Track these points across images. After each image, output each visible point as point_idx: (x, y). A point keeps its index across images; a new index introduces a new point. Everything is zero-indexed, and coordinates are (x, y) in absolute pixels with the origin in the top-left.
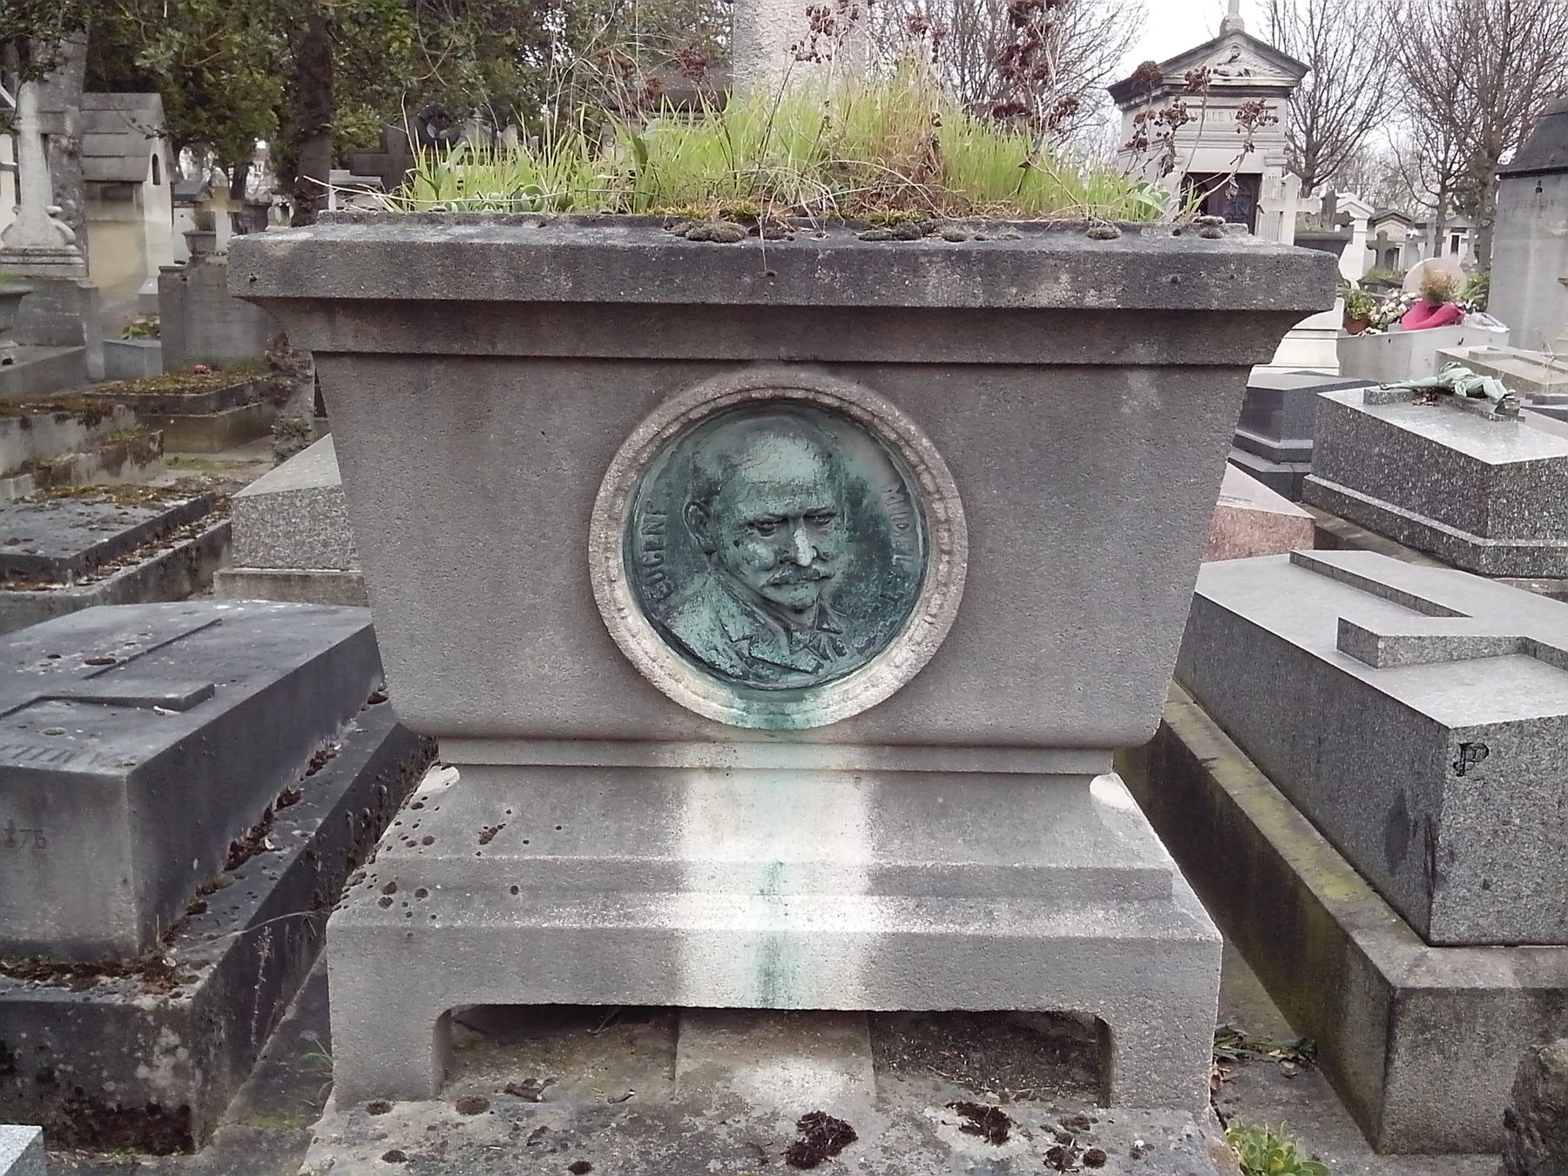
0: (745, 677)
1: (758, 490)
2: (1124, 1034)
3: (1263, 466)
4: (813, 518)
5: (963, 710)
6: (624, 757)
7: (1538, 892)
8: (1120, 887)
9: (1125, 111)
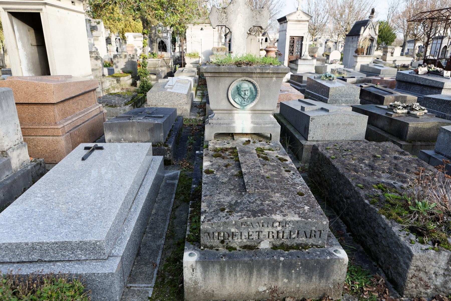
0: (241, 105)
3: (299, 88)
5: (260, 107)
6: (229, 112)
8: (272, 123)
9: (280, 24)
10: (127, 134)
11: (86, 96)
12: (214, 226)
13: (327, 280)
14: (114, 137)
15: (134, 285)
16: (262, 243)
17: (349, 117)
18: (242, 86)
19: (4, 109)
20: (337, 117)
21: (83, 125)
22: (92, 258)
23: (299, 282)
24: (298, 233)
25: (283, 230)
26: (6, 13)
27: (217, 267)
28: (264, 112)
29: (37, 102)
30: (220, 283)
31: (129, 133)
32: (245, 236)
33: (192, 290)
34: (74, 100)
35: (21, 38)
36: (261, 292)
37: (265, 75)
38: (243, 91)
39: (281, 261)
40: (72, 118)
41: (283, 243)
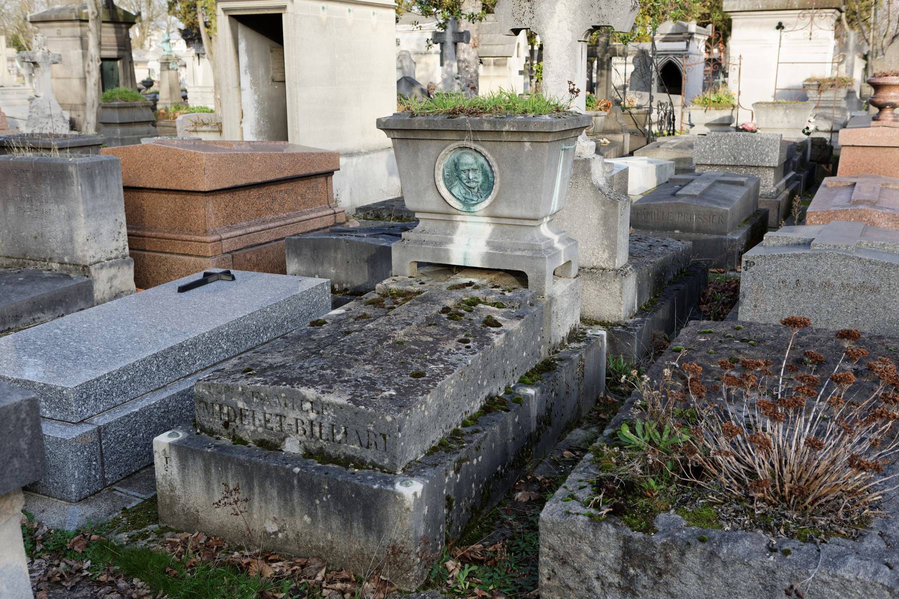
1: (466, 164)
2: (530, 275)
4: (474, 170)
7: (773, 310)
10: (326, 265)
11: (301, 187)
12: (212, 390)
13: (379, 538)
14: (303, 269)
15: (121, 490)
16: (287, 440)
17: (860, 266)
18: (461, 161)
19: (98, 191)
20: (821, 262)
21: (274, 243)
22: (58, 417)
23: (330, 530)
24: (345, 433)
25: (319, 420)
26: (227, 18)
27: (200, 463)
28: (518, 222)
29: (178, 188)
30: (206, 495)
31: (330, 263)
32: (260, 421)
33: (168, 501)
34: (263, 191)
35: (251, 67)
36: (270, 534)
37: (505, 137)
38: (463, 171)
39: (294, 474)
40: (249, 226)
41: (321, 448)
